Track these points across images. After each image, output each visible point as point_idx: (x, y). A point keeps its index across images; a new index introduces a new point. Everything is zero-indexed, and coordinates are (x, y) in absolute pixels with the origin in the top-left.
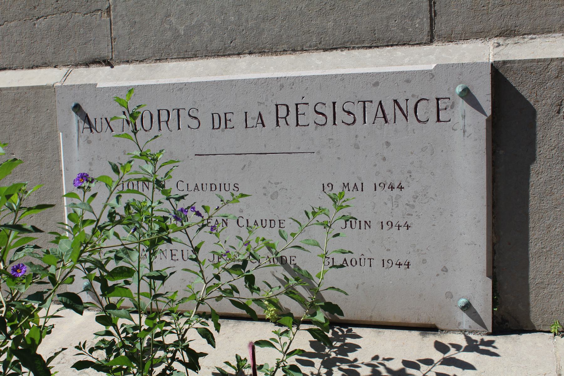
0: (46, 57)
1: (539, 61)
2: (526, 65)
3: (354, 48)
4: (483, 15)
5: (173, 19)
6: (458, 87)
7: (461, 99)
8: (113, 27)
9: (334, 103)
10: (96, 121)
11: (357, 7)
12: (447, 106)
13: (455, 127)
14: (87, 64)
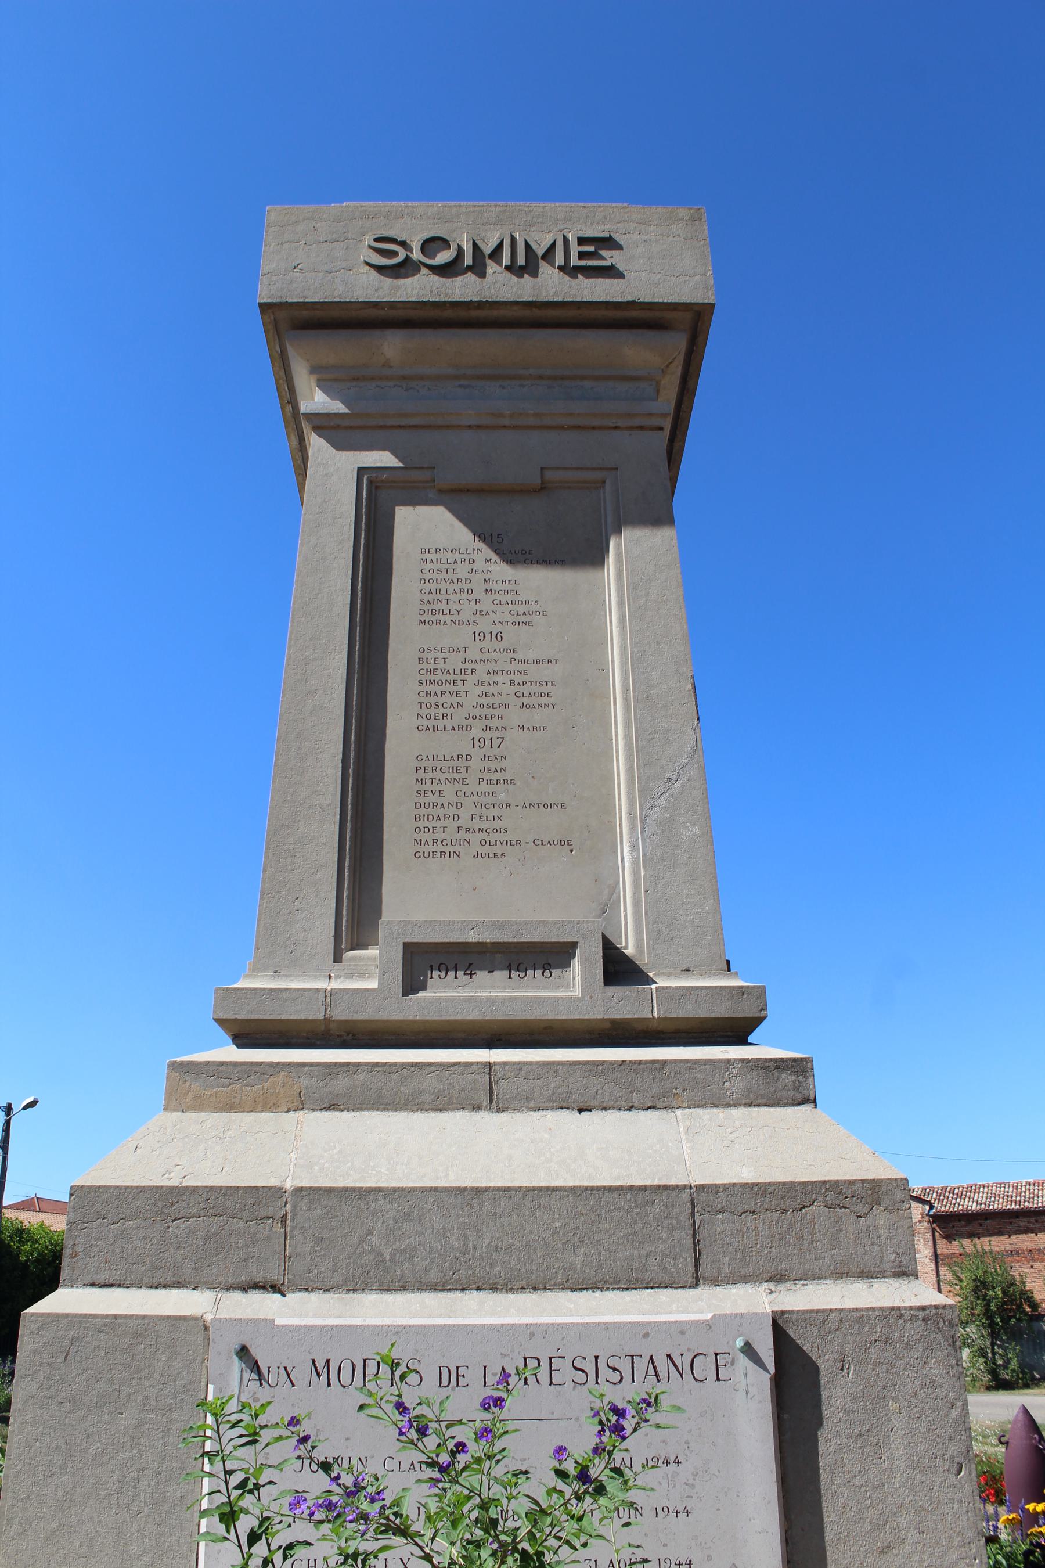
0: (181, 1273)
1: (818, 1311)
2: (805, 1315)
3: (607, 1289)
4: (751, 1257)
5: (375, 1239)
6: (738, 1340)
7: (742, 1354)
8: (288, 1242)
9: (597, 1358)
10: (269, 1371)
11: (611, 1241)
12: (727, 1362)
13: (736, 1388)
14: (244, 1288)
